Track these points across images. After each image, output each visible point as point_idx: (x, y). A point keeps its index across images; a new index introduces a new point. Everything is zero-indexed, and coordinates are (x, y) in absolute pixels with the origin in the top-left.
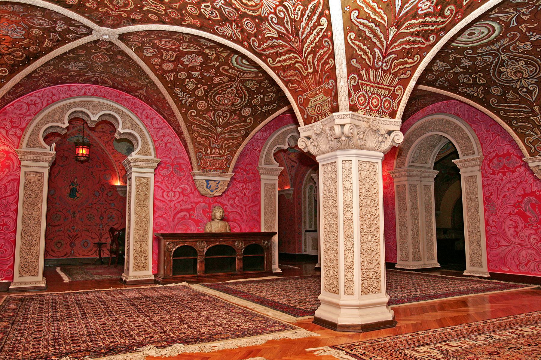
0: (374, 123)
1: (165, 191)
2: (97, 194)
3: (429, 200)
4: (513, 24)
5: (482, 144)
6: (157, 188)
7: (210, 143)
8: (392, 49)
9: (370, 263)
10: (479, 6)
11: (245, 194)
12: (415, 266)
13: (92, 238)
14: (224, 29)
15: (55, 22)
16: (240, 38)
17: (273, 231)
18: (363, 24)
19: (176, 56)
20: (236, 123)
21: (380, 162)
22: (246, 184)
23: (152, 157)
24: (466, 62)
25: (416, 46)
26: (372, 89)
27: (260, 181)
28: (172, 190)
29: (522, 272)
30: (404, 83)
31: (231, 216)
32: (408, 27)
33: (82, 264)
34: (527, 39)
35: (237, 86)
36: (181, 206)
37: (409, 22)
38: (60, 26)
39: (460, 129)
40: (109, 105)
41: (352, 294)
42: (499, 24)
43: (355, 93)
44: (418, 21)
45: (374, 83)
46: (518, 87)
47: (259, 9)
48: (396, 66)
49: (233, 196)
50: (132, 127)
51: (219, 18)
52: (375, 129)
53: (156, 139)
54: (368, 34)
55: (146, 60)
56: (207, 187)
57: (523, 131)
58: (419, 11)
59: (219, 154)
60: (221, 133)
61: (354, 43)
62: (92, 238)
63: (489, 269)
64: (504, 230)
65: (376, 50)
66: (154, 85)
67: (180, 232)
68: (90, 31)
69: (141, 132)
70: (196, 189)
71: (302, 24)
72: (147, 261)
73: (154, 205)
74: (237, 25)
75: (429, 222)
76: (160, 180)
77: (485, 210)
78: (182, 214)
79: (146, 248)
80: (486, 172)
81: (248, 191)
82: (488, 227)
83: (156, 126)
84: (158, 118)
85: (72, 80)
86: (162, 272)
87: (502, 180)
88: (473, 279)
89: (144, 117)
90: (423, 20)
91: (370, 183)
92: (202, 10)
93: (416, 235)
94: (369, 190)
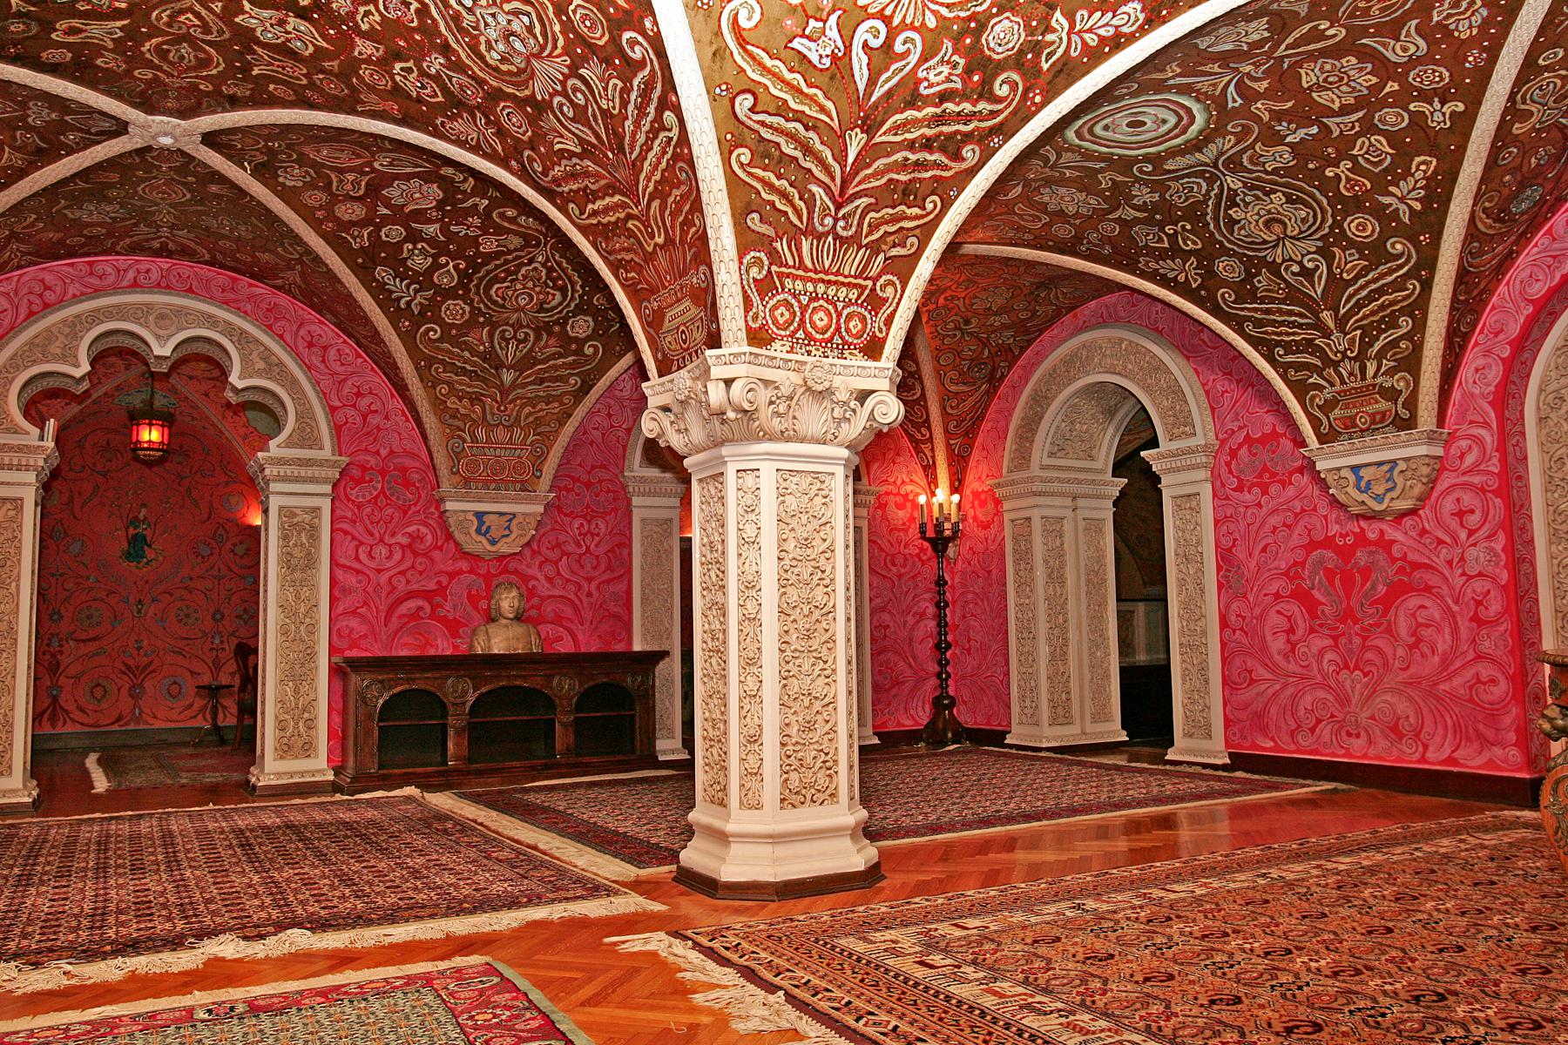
0: (818, 373)
1: (362, 543)
2: (205, 550)
3: (1100, 561)
4: (1234, 101)
5: (1213, 410)
6: (339, 536)
7: (484, 411)
8: (860, 183)
9: (809, 727)
10: (1088, 72)
11: (588, 548)
12: (1055, 738)
13: (192, 673)
15: (24, 106)
16: (500, 149)
18: (771, 127)
19: (367, 184)
20: (553, 357)
21: (840, 471)
22: (589, 522)
23: (327, 452)
24: (1143, 195)
26: (810, 287)
27: (629, 514)
28: (381, 540)
29: (1301, 749)
30: (903, 269)
31: (549, 610)
32: (896, 129)
33: (158, 746)
35: (548, 260)
36: (408, 582)
37: (898, 116)
38: (38, 116)
39: (1160, 367)
40: (203, 313)
41: (758, 807)
42: (1198, 100)
44: (925, 112)
45: (816, 272)
46: (1279, 261)
47: (527, 81)
48: (873, 228)
49: (553, 555)
50: (267, 373)
51: (441, 99)
52: (820, 388)
53: (337, 403)
54: (789, 149)
55: (286, 195)
56: (478, 531)
58: (921, 88)
60: (514, 385)
61: (750, 174)
62: (192, 673)
63: (1227, 745)
64: (1263, 639)
65: (815, 189)
66: (317, 260)
67: (404, 653)
68: (121, 128)
69: (293, 385)
70: (449, 536)
71: (627, 123)
73: (333, 582)
74: (487, 117)
75: (1097, 621)
76: (349, 514)
77: (1220, 586)
78: (412, 604)
79: (312, 696)
80: (1223, 485)
82: (1228, 632)
83: (337, 367)
84: (341, 346)
85: (93, 246)
86: (351, 763)
87: (1259, 505)
88: (1188, 769)
89: (301, 344)
90: (938, 111)
91: (810, 528)
92: (398, 78)
93: (1059, 654)
94: (806, 543)
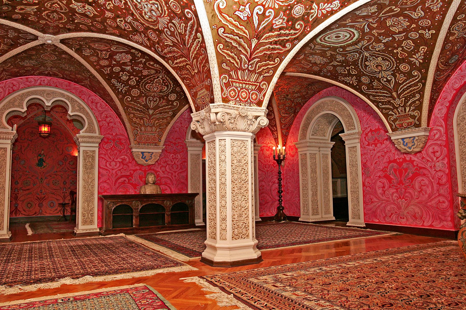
0: (243, 111)
1: (107, 161)
2: (61, 163)
3: (327, 166)
4: (367, 30)
5: (360, 121)
6: (101, 159)
7: (144, 122)
8: (256, 54)
9: (240, 216)
10: (323, 21)
11: (175, 163)
12: (313, 219)
13: (57, 199)
14: (136, 37)
15: (7, 31)
16: (148, 44)
17: (197, 192)
18: (229, 38)
19: (109, 55)
20: (164, 106)
21: (250, 140)
22: (175, 155)
23: (97, 134)
24: (340, 58)
25: (276, 52)
27: (187, 152)
28: (113, 160)
30: (268, 80)
31: (163, 181)
32: (266, 38)
33: (47, 221)
34: (380, 41)
35: (163, 77)
36: (121, 173)
37: (267, 35)
38: (11, 34)
39: (345, 109)
41: (225, 239)
42: (356, 30)
43: (226, 89)
44: (275, 33)
45: (243, 81)
47: (156, 24)
48: (259, 68)
49: (164, 165)
50: (79, 111)
51: (131, 29)
52: (244, 115)
53: (100, 120)
54: (234, 44)
55: (85, 58)
56: (142, 158)
57: (387, 111)
59: (152, 131)
60: (153, 114)
61: (223, 52)
62: (57, 199)
65: (242, 56)
66: (94, 77)
67: (120, 194)
68: (36, 38)
69: (87, 114)
70: (134, 159)
71: (186, 37)
72: (93, 217)
73: (99, 173)
74: (145, 35)
76: (104, 153)
77: (363, 174)
78: (122, 179)
79: (93, 207)
80: (363, 144)
81: (177, 160)
82: (365, 188)
83: (100, 109)
84: (102, 103)
85: (27, 73)
86: (104, 226)
87: (374, 150)
89: (89, 102)
90: (279, 33)
91: (241, 156)
92: (118, 23)
94: (240, 161)
